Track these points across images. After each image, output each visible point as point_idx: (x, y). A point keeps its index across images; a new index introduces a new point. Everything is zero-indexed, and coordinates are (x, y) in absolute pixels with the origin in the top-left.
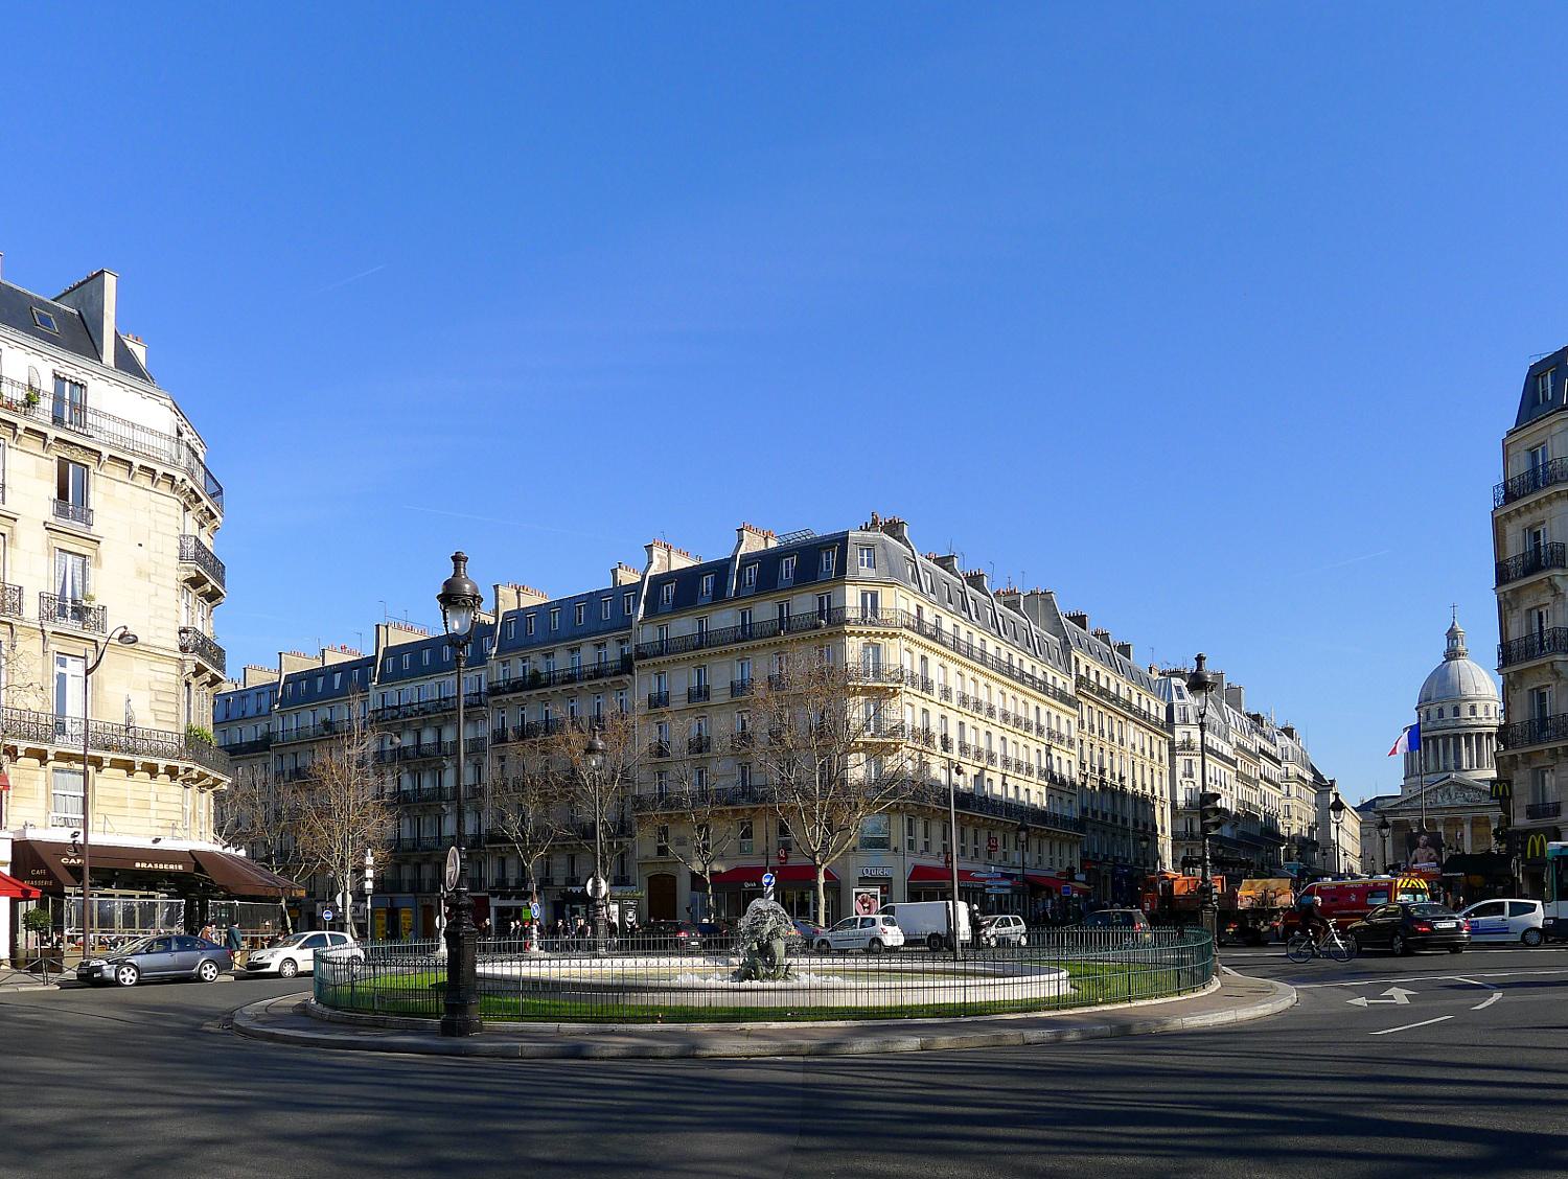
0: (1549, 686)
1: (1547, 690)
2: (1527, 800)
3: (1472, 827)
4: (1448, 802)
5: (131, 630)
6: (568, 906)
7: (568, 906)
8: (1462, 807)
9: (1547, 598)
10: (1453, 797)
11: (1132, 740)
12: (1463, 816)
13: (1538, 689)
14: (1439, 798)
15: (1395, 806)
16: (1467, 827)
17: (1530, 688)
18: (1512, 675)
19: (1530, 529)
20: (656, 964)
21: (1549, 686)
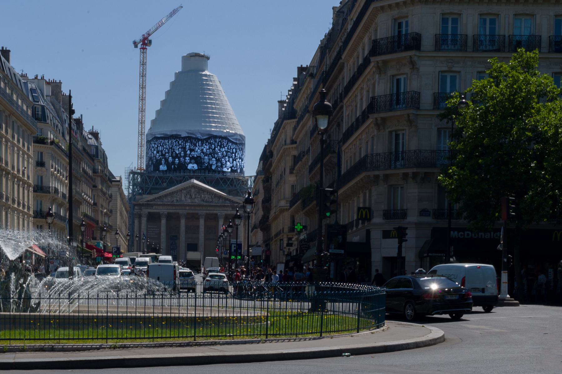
0: (403, 130)
1: (401, 133)
2: (384, 207)
3: (205, 221)
4: (189, 201)
5: (138, 38)
6: (444, 255)
7: (444, 255)
8: (199, 206)
9: (407, 70)
10: (193, 196)
11: (402, 161)
12: (181, 212)
13: (396, 131)
14: (183, 198)
15: (151, 201)
16: (202, 222)
17: (390, 129)
18: (379, 119)
19: (395, 20)
20: (105, 305)
21: (403, 130)
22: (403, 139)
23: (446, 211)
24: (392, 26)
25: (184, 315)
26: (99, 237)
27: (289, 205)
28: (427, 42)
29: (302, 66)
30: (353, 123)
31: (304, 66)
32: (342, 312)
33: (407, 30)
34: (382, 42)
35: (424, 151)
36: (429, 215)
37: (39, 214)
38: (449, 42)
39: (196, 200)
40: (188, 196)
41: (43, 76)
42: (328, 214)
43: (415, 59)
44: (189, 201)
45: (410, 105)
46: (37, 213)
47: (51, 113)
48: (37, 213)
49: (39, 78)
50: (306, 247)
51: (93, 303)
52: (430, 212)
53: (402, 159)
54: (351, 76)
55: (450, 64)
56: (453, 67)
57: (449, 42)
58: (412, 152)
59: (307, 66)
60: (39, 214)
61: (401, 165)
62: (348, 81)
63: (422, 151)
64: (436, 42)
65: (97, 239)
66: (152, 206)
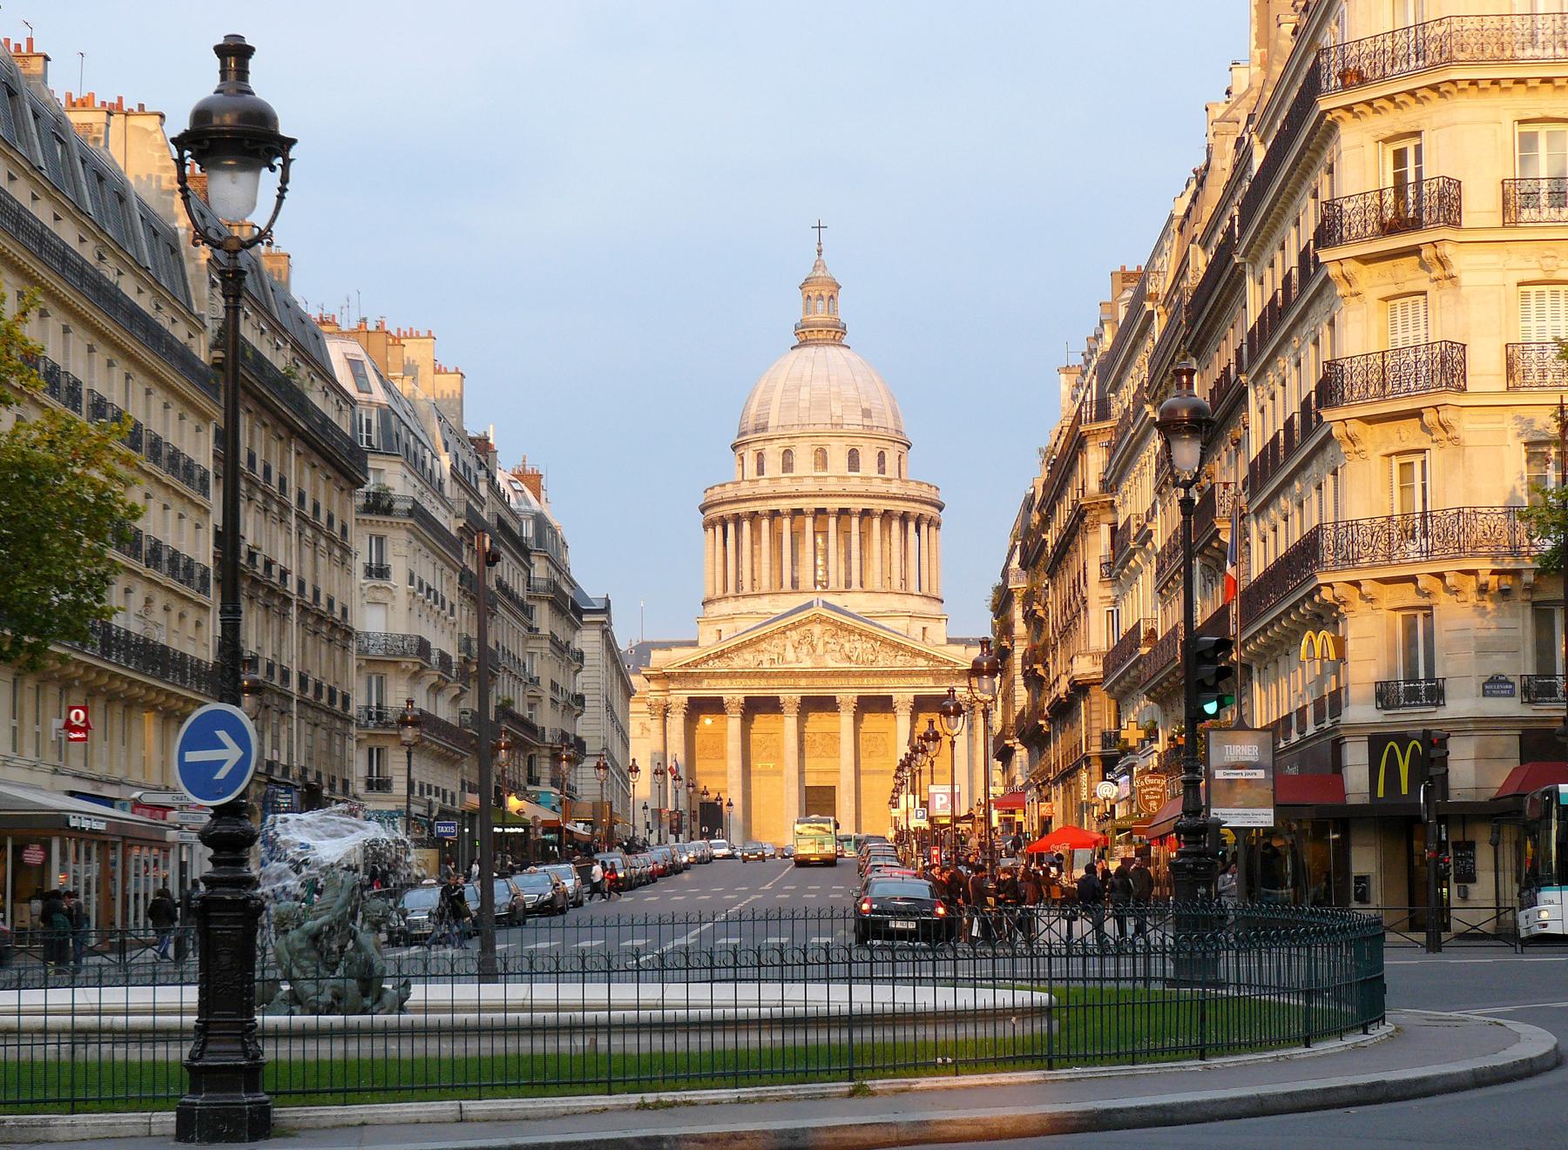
15: (696, 664)
21: (1423, 451)
22: (1424, 478)
23: (1561, 678)
24: (1293, 326)
25: (679, 1012)
26: (548, 776)
27: (1100, 668)
28: (1480, 206)
29: (1123, 268)
30: (1292, 417)
31: (1131, 268)
32: (1279, 988)
33: (1419, 172)
34: (1347, 207)
35: (1485, 510)
36: (1512, 695)
37: (374, 716)
38: (1544, 200)
39: (828, 657)
40: (805, 648)
41: (383, 323)
42: (1210, 708)
43: (1447, 250)
44: (807, 664)
45: (1436, 380)
46: (370, 714)
47: (420, 442)
48: (370, 714)
49: (371, 327)
50: (1156, 793)
51: (1126, 985)
52: (1513, 684)
53: (1425, 534)
54: (1266, 303)
55: (1549, 261)
56: (1559, 268)
57: (1544, 200)
58: (1450, 512)
59: (1139, 268)
60: (374, 716)
61: (1421, 552)
62: (1259, 312)
63: (1479, 510)
64: (1505, 202)
65: (542, 780)
66: (699, 677)
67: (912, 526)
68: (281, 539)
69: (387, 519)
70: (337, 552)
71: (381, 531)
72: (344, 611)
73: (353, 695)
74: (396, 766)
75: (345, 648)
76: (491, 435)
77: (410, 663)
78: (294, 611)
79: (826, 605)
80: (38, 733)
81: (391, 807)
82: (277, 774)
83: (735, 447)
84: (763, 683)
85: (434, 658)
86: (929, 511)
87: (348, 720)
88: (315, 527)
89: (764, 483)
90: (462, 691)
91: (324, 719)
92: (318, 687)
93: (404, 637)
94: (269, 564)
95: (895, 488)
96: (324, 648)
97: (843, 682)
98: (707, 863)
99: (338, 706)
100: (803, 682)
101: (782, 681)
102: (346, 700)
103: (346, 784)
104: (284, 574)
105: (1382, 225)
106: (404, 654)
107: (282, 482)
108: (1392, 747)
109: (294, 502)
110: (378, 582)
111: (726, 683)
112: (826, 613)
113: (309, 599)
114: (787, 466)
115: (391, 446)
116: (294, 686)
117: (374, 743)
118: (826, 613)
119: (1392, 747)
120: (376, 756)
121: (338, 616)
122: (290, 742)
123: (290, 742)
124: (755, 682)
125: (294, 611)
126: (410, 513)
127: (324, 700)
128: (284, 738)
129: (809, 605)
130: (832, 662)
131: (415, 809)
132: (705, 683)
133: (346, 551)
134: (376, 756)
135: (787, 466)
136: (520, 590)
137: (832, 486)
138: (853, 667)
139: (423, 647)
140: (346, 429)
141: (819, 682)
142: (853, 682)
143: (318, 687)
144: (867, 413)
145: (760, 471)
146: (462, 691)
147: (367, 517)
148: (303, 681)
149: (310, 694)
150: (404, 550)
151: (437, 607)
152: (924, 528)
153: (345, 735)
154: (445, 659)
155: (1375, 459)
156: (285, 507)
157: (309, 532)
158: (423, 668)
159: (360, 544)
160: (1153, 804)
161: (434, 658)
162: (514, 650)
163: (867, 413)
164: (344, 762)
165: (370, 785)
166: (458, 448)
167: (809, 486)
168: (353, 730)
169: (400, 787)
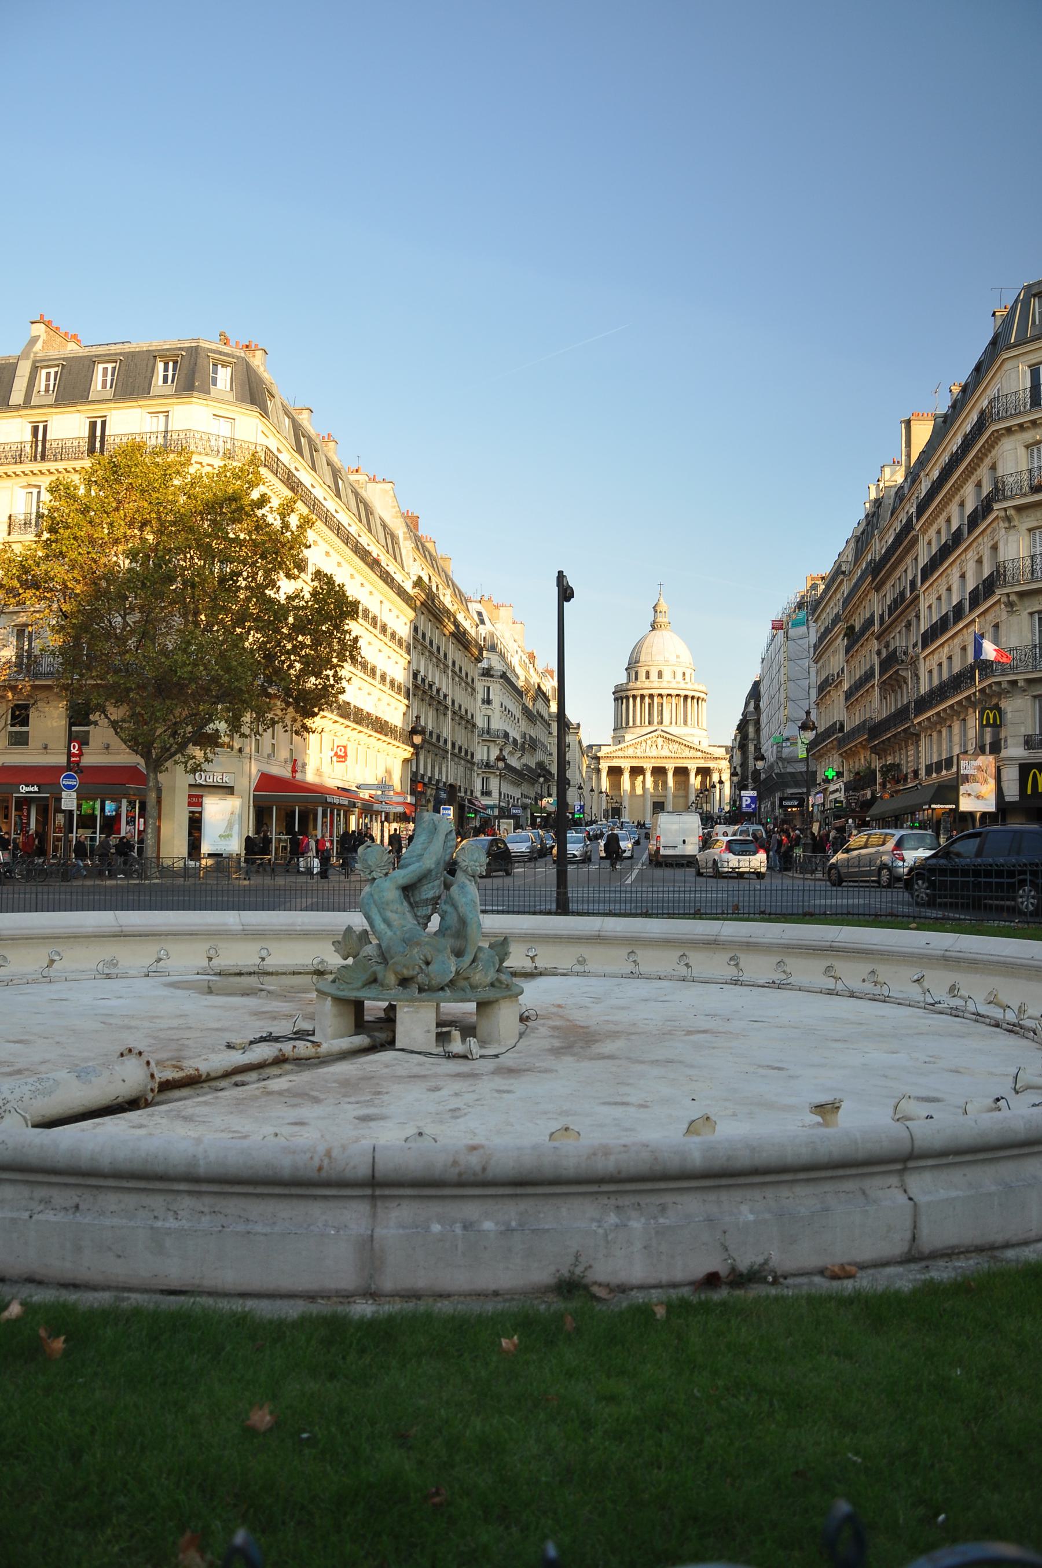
67: (695, 701)
68: (444, 680)
69: (492, 679)
70: (469, 690)
71: (488, 684)
72: (472, 715)
73: (475, 754)
74: (494, 784)
75: (473, 732)
76: (535, 652)
77: (500, 741)
78: (449, 713)
79: (662, 731)
80: (273, 744)
81: (491, 803)
82: (441, 785)
83: (626, 669)
84: (637, 760)
85: (511, 740)
86: (702, 695)
87: (473, 764)
88: (459, 677)
89: (638, 683)
90: (522, 755)
91: (463, 762)
92: (460, 748)
93: (498, 730)
94: (438, 691)
95: (689, 686)
96: (463, 731)
97: (668, 760)
98: (447, 834)
99: (469, 757)
100: (653, 760)
101: (645, 760)
102: (472, 755)
103: (472, 792)
104: (445, 696)
105: (1031, 488)
106: (498, 737)
107: (445, 655)
108: (1035, 772)
109: (450, 665)
110: (487, 706)
111: (622, 760)
112: (663, 734)
113: (457, 708)
114: (648, 677)
115: (493, 648)
116: (449, 746)
117: (484, 775)
118: (663, 734)
119: (1035, 772)
120: (485, 781)
121: (470, 717)
122: (447, 771)
123: (447, 771)
124: (633, 760)
125: (449, 713)
126: (501, 677)
127: (463, 754)
128: (444, 769)
129: (656, 730)
130: (665, 753)
131: (502, 804)
132: (614, 760)
133: (474, 689)
134: (485, 781)
135: (648, 677)
136: (546, 717)
137: (665, 685)
138: (673, 755)
139: (506, 735)
140: (473, 634)
141: (659, 760)
142: (672, 761)
143: (460, 748)
144: (678, 657)
145: (636, 679)
146: (522, 755)
147: (483, 678)
148: (453, 745)
149: (456, 751)
150: (498, 692)
151: (512, 719)
152: (700, 701)
153: (471, 770)
154: (515, 740)
155: (1025, 614)
156: (447, 666)
157: (457, 679)
158: (506, 743)
159: (480, 686)
160: (853, 804)
161: (511, 740)
162: (543, 741)
163: (678, 657)
164: (471, 782)
165: (483, 793)
166: (522, 654)
167: (656, 685)
168: (476, 768)
169: (495, 794)
